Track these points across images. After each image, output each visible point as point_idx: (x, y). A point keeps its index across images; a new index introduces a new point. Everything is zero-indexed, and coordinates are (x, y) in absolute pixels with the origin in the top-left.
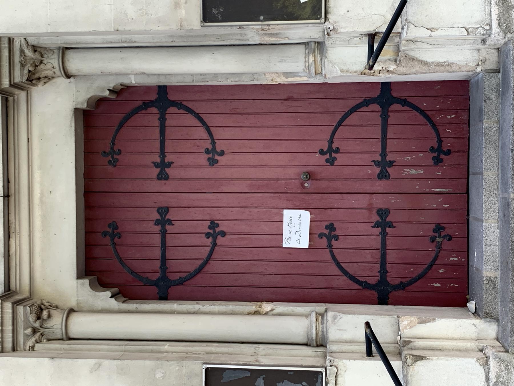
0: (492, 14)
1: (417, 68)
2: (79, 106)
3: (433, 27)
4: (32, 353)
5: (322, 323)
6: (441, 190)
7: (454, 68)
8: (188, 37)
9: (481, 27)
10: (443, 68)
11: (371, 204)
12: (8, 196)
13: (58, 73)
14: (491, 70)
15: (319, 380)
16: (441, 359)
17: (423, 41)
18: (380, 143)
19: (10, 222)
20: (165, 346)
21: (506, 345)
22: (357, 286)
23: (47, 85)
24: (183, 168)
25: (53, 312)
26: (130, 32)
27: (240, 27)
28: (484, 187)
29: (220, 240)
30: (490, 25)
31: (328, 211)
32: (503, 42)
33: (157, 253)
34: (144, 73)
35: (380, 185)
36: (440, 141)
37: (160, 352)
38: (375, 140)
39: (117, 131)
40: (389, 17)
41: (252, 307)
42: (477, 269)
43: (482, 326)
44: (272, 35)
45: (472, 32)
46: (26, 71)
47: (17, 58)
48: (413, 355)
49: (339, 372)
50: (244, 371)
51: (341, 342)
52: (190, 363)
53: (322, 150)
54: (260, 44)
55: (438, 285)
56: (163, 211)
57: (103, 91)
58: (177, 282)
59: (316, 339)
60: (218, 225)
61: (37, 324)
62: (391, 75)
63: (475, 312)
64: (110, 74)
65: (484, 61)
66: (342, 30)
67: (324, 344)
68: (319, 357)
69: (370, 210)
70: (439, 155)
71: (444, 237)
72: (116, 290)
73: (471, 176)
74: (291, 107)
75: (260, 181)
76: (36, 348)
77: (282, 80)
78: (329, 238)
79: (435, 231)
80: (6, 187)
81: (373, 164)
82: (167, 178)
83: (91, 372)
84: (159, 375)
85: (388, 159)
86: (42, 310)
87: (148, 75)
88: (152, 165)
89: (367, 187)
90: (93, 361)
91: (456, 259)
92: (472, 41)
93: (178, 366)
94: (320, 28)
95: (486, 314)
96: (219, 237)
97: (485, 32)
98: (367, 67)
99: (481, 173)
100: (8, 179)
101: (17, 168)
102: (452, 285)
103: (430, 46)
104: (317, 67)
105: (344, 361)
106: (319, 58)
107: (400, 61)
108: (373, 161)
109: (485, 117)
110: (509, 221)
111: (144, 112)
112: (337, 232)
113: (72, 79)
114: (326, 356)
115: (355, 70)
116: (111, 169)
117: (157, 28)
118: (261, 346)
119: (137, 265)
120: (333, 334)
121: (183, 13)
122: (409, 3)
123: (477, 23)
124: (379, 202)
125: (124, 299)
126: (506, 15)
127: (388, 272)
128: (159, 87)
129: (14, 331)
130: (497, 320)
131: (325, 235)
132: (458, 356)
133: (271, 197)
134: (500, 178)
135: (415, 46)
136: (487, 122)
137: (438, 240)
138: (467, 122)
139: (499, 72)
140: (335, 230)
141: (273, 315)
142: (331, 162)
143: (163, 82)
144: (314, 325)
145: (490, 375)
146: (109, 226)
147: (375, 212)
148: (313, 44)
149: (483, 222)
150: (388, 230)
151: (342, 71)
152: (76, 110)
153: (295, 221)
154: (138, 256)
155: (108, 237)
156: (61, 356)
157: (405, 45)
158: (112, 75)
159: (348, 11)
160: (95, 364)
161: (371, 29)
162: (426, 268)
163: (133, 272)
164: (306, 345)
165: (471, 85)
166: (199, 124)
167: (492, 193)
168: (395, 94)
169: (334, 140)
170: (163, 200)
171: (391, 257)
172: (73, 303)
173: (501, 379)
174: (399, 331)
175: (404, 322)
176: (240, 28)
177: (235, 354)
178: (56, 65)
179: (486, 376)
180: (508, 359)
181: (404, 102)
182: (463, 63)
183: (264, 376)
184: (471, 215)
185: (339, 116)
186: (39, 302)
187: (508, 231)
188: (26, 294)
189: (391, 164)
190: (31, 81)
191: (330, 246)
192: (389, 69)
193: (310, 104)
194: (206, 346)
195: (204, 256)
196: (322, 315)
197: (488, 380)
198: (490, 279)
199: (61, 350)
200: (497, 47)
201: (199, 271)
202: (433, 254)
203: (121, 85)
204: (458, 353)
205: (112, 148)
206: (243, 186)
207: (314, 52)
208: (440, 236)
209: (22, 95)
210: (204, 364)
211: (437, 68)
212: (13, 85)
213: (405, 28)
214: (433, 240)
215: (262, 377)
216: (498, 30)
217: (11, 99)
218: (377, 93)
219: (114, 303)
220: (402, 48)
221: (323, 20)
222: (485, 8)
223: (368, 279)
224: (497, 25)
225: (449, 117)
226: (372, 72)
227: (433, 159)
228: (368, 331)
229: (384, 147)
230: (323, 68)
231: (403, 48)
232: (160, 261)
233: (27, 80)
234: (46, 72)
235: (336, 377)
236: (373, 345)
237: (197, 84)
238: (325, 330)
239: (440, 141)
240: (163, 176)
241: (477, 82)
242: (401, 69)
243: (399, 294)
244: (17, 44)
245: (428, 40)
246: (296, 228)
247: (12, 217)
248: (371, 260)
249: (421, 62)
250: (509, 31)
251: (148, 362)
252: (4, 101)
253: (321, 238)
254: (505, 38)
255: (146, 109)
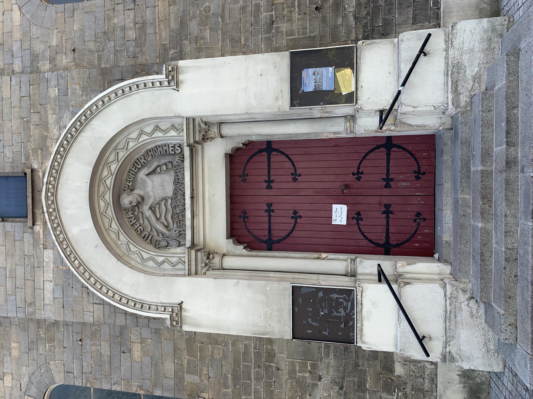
0: (448, 98)
1: (406, 128)
2: (227, 152)
3: (415, 106)
4: (205, 276)
5: (354, 264)
6: (420, 194)
7: (427, 128)
8: (282, 115)
9: (442, 105)
10: (421, 128)
11: (381, 202)
12: (193, 197)
13: (217, 136)
14: (447, 128)
15: (353, 294)
16: (420, 284)
17: (410, 113)
18: (386, 169)
19: (194, 211)
20: (271, 274)
21: (456, 277)
22: (373, 245)
23: (212, 141)
24: (279, 183)
25: (215, 255)
26: (253, 114)
27: (310, 109)
28: (444, 192)
29: (299, 220)
30: (447, 104)
31: (357, 205)
32: (455, 113)
33: (266, 226)
34: (260, 135)
35: (386, 191)
36: (419, 167)
37: (269, 277)
38: (383, 168)
39: (246, 165)
40: (391, 101)
41: (316, 255)
42: (440, 237)
43: (442, 267)
44: (327, 112)
45: (437, 108)
46: (201, 135)
47: (197, 128)
48: (404, 282)
49: (363, 290)
50: (312, 288)
51: (364, 274)
52: (284, 283)
53: (354, 173)
54: (321, 118)
55: (418, 245)
56: (270, 205)
57: (239, 143)
58: (276, 242)
59: (351, 272)
60: (297, 212)
61: (207, 261)
62: (392, 132)
63: (438, 259)
64: (243, 136)
65: (444, 124)
66: (365, 109)
67: (355, 275)
68: (352, 282)
69: (380, 205)
70: (418, 175)
71: (421, 219)
72: (246, 245)
73: (436, 186)
74: (337, 150)
75: (320, 190)
76: (207, 273)
77: (332, 136)
78: (358, 220)
79: (416, 216)
80: (192, 193)
81: (382, 180)
82: (271, 188)
83: (234, 286)
84: (268, 289)
85: (390, 177)
86: (210, 254)
87: (262, 135)
88: (264, 181)
89: (379, 192)
90: (235, 281)
91: (428, 231)
92: (437, 113)
93: (449, 8)
94: (353, 108)
95: (445, 260)
96: (298, 218)
97: (444, 108)
98: (379, 128)
99: (442, 184)
100: (193, 189)
101: (197, 183)
102: (425, 245)
103: (414, 116)
104: (351, 129)
105: (366, 284)
106: (352, 124)
107: (397, 124)
108: (382, 178)
109: (445, 154)
110: (458, 210)
111: (260, 154)
112: (362, 217)
113: (224, 139)
114: (356, 281)
115: (372, 130)
116: (243, 184)
117: (267, 111)
118: (321, 275)
119: (256, 233)
120: (360, 270)
121: (280, 103)
122: (402, 93)
123: (440, 103)
124: (385, 200)
125: (250, 250)
126: (457, 99)
127: (390, 238)
128: (267, 141)
129: (196, 265)
130: (451, 264)
131: (355, 218)
132: (429, 283)
133: (326, 198)
134: (453, 187)
135: (405, 116)
136: (446, 157)
137: (418, 220)
138: (434, 157)
139: (452, 129)
140: (360, 215)
141: (327, 259)
142: (359, 179)
143: (270, 139)
144: (349, 265)
145: (447, 293)
146: (242, 213)
147: (383, 205)
148: (349, 116)
149: (443, 211)
150: (390, 215)
151: (365, 131)
152: (226, 154)
153: (339, 210)
154: (256, 228)
155: (242, 218)
156: (219, 277)
157: (399, 116)
158: (244, 136)
159: (368, 99)
160: (236, 282)
161: (381, 108)
162: (411, 236)
163: (254, 236)
164: (345, 275)
165: (436, 137)
166: (288, 160)
167: (448, 195)
168: (394, 143)
169: (360, 168)
170: (269, 200)
171: (391, 230)
172: (225, 251)
173: (453, 296)
174: (396, 269)
175: (399, 264)
176: (310, 109)
177: (308, 279)
178: (216, 132)
179: (445, 294)
180: (457, 285)
181: (399, 147)
182: (432, 125)
183: (323, 291)
184: (436, 207)
185: (363, 155)
186: (208, 250)
187: (458, 216)
188: (202, 246)
189: (392, 180)
190: (204, 140)
191: (358, 224)
192: (391, 129)
193: (347, 148)
194: (292, 275)
195: (291, 229)
196: (354, 260)
197: (446, 296)
198: (447, 242)
199: (219, 274)
200: (451, 116)
201: (288, 236)
202: (415, 228)
203: (248, 141)
204: (429, 281)
205: (244, 173)
206: (311, 192)
207: (350, 121)
208: (419, 219)
209: (200, 147)
210: (291, 283)
211: (418, 128)
212: (195, 142)
213: (400, 107)
214: (415, 221)
215: (322, 292)
216: (452, 107)
217: (194, 149)
218: (384, 142)
219: (245, 252)
220: (398, 117)
221: (355, 104)
222: (444, 95)
223: (378, 241)
224: (451, 104)
225: (424, 154)
226: (382, 130)
227: (415, 177)
228: (379, 269)
229: (388, 171)
230: (355, 129)
231: (399, 118)
232: (268, 231)
233: (202, 139)
234: (211, 135)
235: (361, 292)
236: (382, 276)
237: (287, 139)
238: (355, 268)
239: (419, 167)
240: (269, 187)
241: (440, 135)
242: (398, 129)
243: (396, 249)
244: (197, 121)
245: (412, 113)
246: (340, 214)
247: (195, 208)
248: (381, 231)
249: (409, 125)
250: (458, 107)
251: (262, 282)
252: (191, 150)
253: (353, 219)
254: (456, 111)
255: (261, 153)
